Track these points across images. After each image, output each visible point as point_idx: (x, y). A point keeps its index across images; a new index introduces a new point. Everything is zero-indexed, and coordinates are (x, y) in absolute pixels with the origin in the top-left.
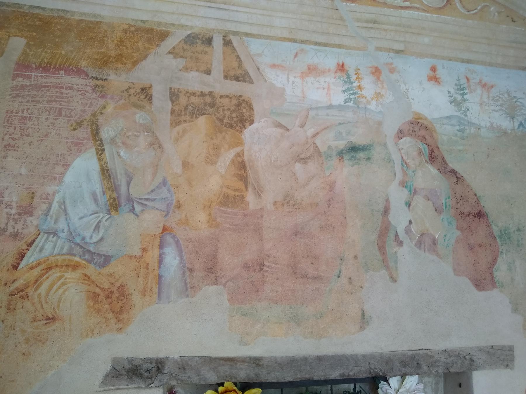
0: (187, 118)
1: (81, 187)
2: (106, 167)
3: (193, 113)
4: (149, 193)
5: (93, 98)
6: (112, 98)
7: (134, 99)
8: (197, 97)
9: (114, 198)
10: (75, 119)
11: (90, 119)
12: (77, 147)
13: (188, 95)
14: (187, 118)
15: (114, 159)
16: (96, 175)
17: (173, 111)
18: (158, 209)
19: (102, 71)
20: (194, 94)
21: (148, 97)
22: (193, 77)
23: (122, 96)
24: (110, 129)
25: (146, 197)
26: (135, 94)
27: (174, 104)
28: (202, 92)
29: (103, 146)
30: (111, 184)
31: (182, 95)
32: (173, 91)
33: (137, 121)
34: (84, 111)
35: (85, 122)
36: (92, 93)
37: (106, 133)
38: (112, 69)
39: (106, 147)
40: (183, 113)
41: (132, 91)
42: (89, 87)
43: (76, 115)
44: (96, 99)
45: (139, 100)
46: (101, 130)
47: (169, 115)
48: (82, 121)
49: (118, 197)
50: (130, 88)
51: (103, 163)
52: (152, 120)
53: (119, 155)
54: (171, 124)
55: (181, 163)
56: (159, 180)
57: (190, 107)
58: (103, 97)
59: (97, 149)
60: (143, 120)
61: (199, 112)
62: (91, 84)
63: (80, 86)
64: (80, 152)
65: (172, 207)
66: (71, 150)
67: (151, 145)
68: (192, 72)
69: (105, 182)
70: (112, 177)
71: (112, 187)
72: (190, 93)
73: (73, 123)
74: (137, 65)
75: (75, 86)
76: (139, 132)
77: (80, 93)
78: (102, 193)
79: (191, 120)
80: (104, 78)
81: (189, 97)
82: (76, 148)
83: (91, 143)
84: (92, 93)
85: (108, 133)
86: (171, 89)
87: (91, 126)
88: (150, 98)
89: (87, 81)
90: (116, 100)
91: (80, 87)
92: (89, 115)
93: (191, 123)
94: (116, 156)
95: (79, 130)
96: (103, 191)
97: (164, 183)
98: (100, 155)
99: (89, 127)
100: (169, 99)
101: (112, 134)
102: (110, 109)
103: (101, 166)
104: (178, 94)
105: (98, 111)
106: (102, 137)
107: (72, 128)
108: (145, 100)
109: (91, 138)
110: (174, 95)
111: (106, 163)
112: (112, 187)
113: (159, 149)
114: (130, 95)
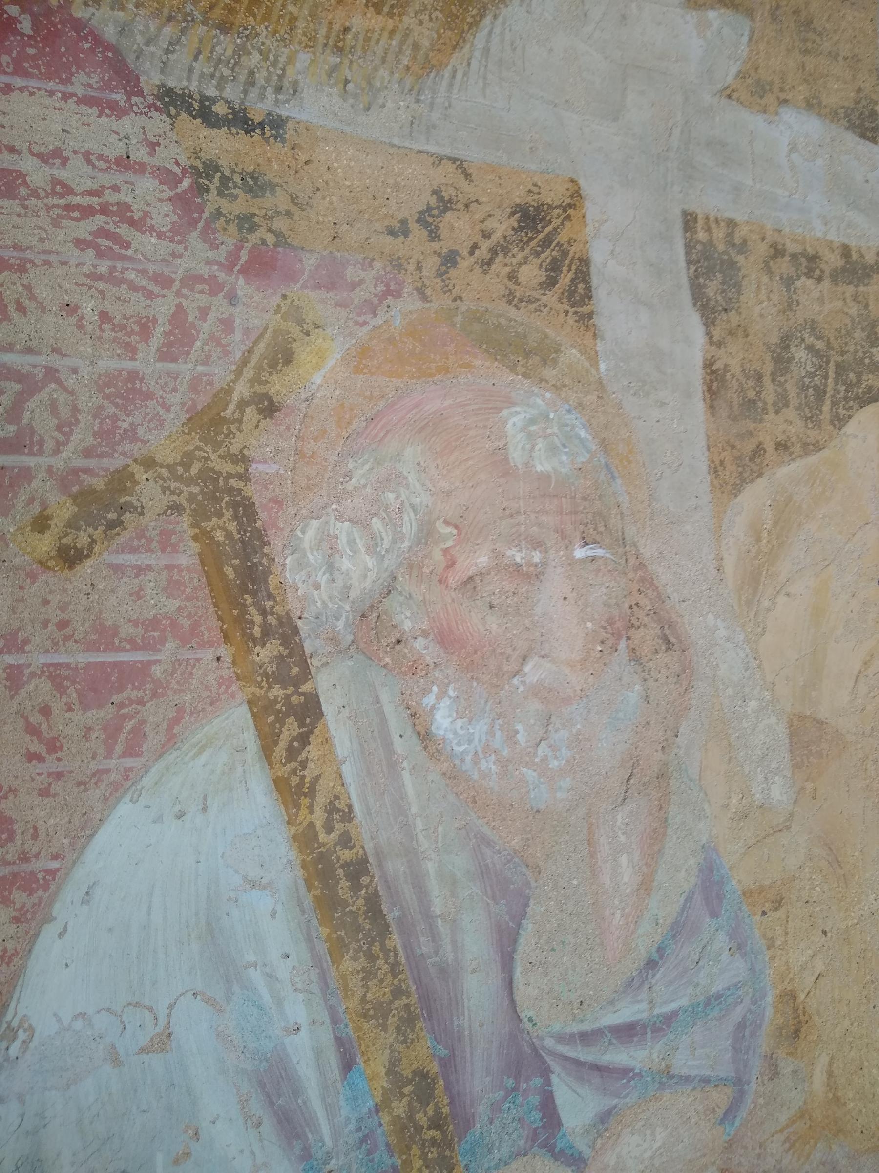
0: (786, 424)
1: (164, 1041)
2: (346, 841)
3: (820, 393)
4: (632, 986)
5: (192, 280)
6: (330, 280)
7: (480, 288)
8: (826, 284)
9: (422, 1075)
10: (58, 462)
11: (187, 460)
12: (106, 713)
13: (783, 266)
14: (786, 424)
15: (393, 767)
16: (274, 929)
17: (715, 379)
18: (687, 1079)
19: (241, 51)
20: (810, 263)
21: (565, 279)
22: (793, 148)
23: (397, 264)
24: (342, 530)
25: (626, 1012)
26: (483, 252)
27: (717, 334)
28: (846, 251)
29: (306, 673)
30: (395, 969)
31: (750, 267)
32: (702, 235)
33: (516, 456)
34: (128, 390)
35: (149, 492)
36: (178, 233)
37: (323, 565)
38: (310, 42)
39: (331, 685)
40: (770, 393)
41: (459, 228)
42: (147, 185)
43: (65, 428)
44: (215, 287)
45: (510, 298)
46: (276, 543)
47: (699, 406)
48: (121, 481)
49: (448, 1064)
50: (446, 205)
51: (319, 817)
52: (604, 445)
53: (425, 737)
54: (716, 469)
55: (782, 730)
56: (679, 876)
57: (800, 354)
58: (262, 266)
59: (260, 710)
60: (553, 450)
61: (849, 386)
62: (165, 157)
63: (77, 162)
64: (131, 751)
65: (764, 1043)
66: (53, 746)
67: (618, 630)
68: (789, 115)
69: (348, 964)
70: (391, 915)
71: (398, 993)
72: (794, 256)
73: (54, 498)
74: (475, 24)
75: (28, 165)
76: (538, 544)
77: (84, 229)
78: (333, 1061)
79: (813, 434)
80: (258, 110)
81: (788, 282)
82: (94, 715)
83: (212, 661)
84: (178, 233)
85: (331, 567)
86: (689, 221)
87: (200, 515)
88: (574, 283)
89: (128, 125)
90: (359, 295)
91: (77, 174)
92: (175, 419)
93: (813, 459)
94: (404, 745)
95: (106, 556)
96: (340, 1041)
97: (710, 887)
98: (292, 753)
99: (185, 521)
100: (686, 296)
101: (360, 569)
102: (321, 371)
103: (305, 839)
104: (732, 264)
105: (242, 390)
106: (293, 606)
107: (45, 544)
108: (551, 298)
109: (211, 625)
110: (712, 265)
111: (340, 812)
112: (398, 993)
113: (662, 658)
114: (450, 260)
